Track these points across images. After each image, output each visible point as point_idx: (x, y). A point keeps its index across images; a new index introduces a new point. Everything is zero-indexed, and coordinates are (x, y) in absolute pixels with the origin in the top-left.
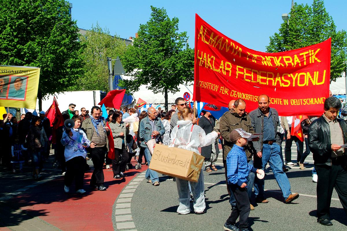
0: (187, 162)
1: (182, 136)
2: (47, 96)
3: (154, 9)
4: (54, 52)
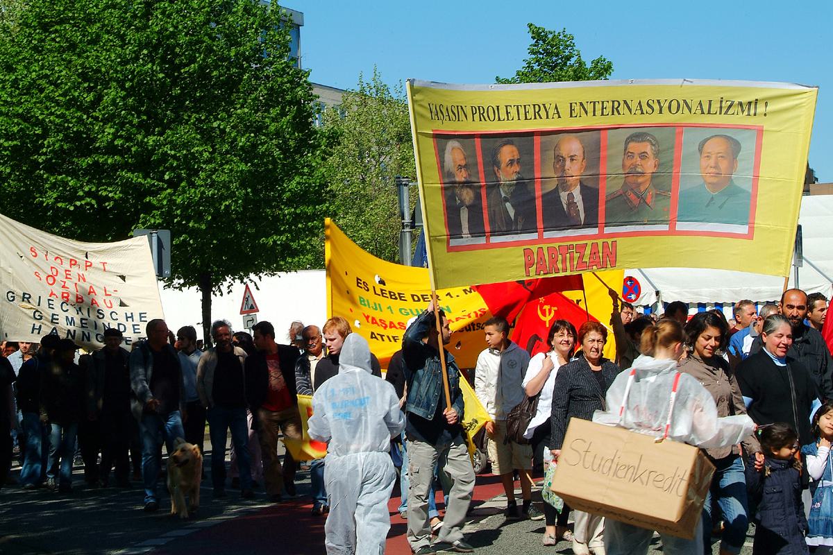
0: (676, 478)
1: (643, 401)
2: (226, 284)
3: (539, 35)
4: (249, 153)
